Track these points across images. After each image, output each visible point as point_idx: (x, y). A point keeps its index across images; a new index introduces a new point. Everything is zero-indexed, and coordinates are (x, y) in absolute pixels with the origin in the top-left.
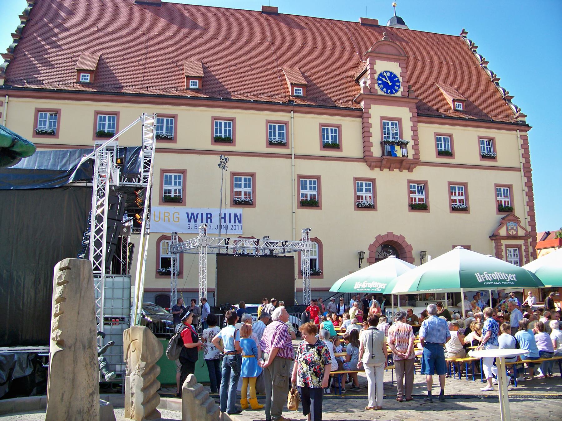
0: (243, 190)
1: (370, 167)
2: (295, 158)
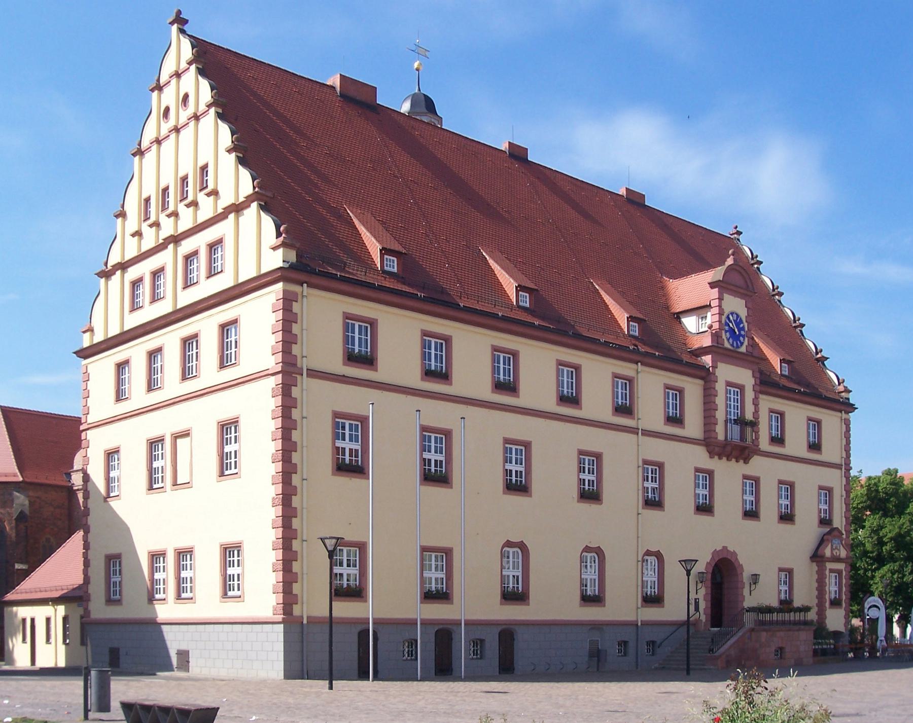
1: (710, 453)
2: (308, 375)
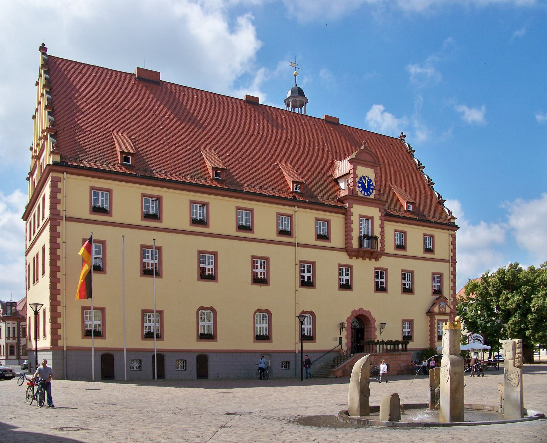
0: (207, 266)
2: (66, 220)
